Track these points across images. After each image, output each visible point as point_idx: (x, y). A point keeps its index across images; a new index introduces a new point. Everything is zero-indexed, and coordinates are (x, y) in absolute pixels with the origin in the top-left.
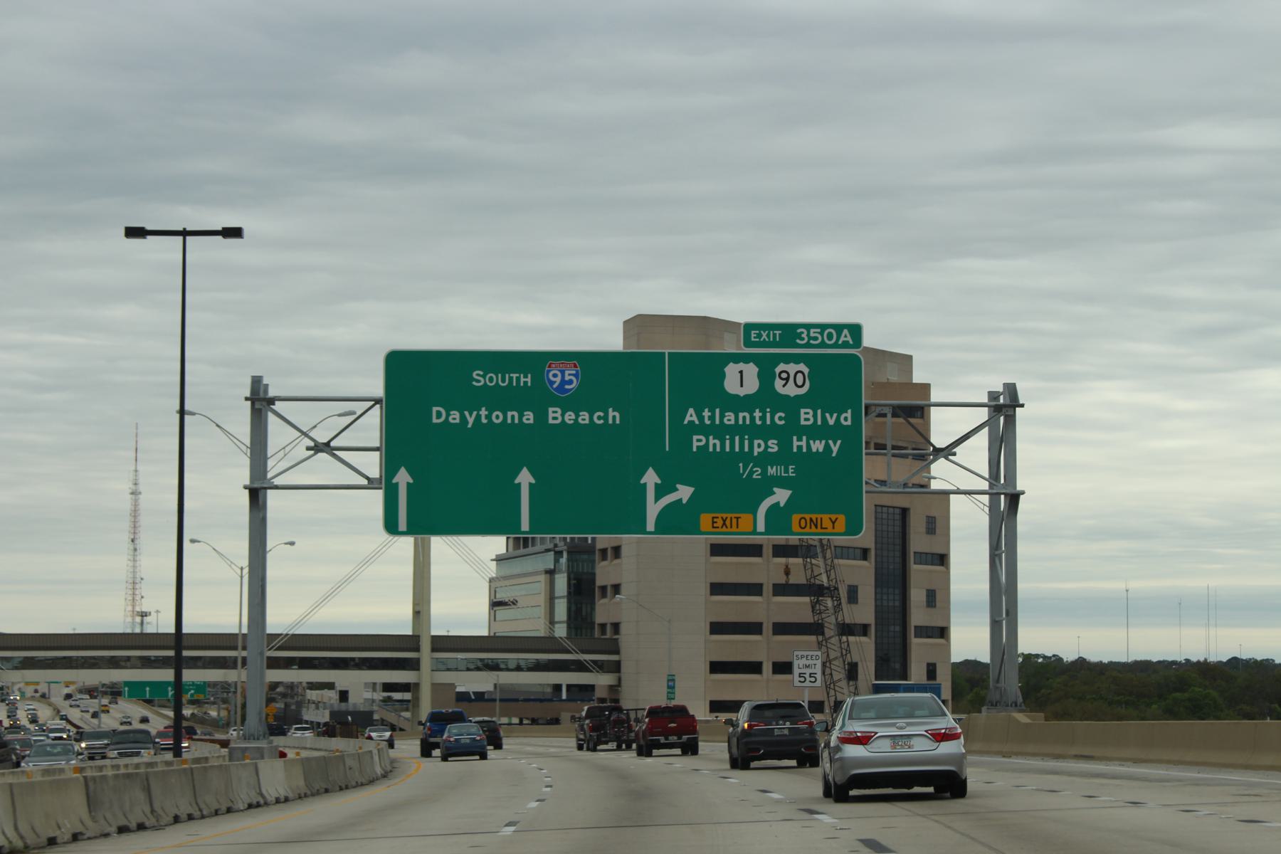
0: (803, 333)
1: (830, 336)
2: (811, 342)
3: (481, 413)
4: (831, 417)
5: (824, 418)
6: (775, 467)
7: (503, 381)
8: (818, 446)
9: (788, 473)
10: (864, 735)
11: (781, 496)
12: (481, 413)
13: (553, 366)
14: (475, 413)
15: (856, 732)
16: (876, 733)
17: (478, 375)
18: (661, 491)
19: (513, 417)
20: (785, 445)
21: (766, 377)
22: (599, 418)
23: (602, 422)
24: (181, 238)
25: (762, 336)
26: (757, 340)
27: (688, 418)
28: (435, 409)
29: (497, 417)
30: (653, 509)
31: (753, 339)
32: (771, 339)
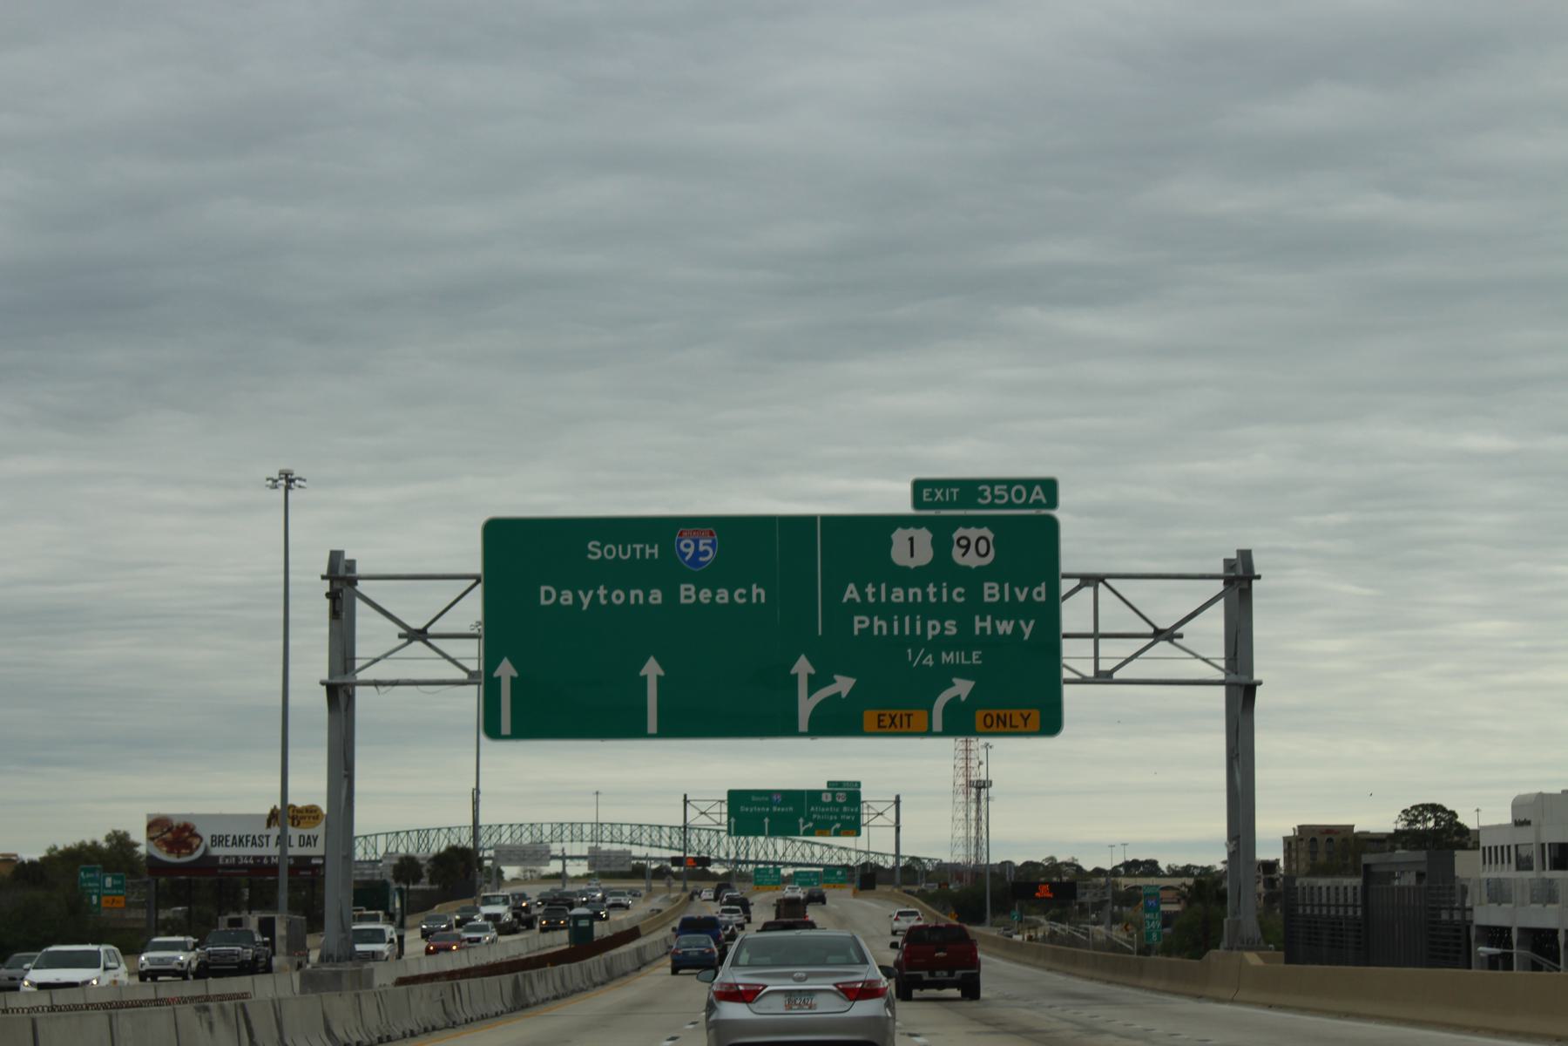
2: (997, 501)
4: (1021, 592)
5: (1012, 594)
6: (952, 654)
7: (625, 553)
9: (971, 659)
10: (748, 988)
11: (962, 688)
13: (685, 534)
14: (591, 593)
15: (737, 985)
16: (765, 986)
17: (594, 546)
18: (815, 684)
19: (637, 597)
20: (965, 625)
21: (942, 545)
22: (741, 596)
23: (744, 600)
24: (1101, 630)
25: (936, 495)
26: (931, 500)
27: (847, 596)
28: (543, 589)
29: (618, 597)
30: (806, 706)
32: (947, 499)
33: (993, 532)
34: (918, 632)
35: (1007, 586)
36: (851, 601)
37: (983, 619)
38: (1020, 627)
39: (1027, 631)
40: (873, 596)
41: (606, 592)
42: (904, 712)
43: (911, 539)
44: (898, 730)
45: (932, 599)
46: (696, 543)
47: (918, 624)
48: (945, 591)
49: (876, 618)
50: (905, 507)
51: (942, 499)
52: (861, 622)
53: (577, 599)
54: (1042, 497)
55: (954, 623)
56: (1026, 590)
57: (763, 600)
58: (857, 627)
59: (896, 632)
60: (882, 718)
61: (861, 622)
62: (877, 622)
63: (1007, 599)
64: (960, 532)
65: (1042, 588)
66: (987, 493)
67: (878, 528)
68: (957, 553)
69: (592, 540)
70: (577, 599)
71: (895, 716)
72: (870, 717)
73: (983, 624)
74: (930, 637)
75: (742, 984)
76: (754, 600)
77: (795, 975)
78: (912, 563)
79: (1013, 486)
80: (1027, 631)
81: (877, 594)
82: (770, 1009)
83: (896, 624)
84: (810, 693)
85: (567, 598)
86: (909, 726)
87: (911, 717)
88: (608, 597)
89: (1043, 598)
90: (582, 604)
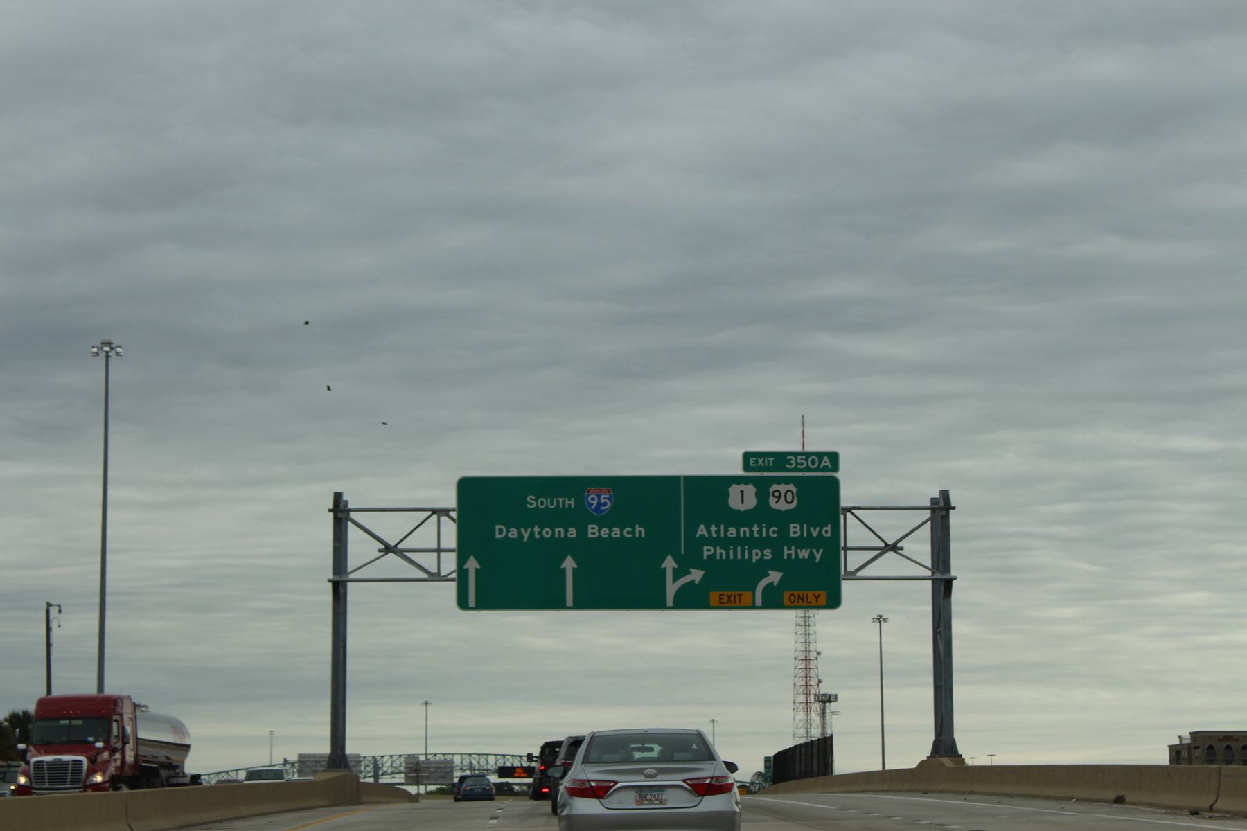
0: (791, 459)
1: (813, 462)
2: (799, 467)
3: (534, 530)
4: (815, 530)
5: (809, 531)
7: (552, 504)
8: (804, 554)
10: (600, 784)
11: (775, 577)
12: (534, 530)
14: (529, 530)
15: (589, 781)
16: (616, 783)
17: (531, 499)
18: (677, 574)
19: (559, 532)
20: (777, 552)
21: (762, 495)
22: (628, 532)
23: (630, 536)
25: (758, 462)
27: (699, 533)
28: (497, 527)
29: (547, 533)
30: (671, 589)
31: (752, 465)
32: (766, 465)
33: (796, 487)
34: (747, 557)
35: (805, 526)
36: (702, 536)
37: (789, 549)
38: (813, 553)
39: (818, 557)
40: (758, 533)
41: (539, 530)
42: (736, 593)
43: (742, 492)
44: (733, 605)
45: (756, 535)
46: (599, 497)
47: (746, 551)
48: (764, 529)
49: (718, 548)
50: (739, 471)
51: (763, 465)
52: (708, 550)
53: (520, 534)
54: (828, 464)
55: (770, 551)
56: (818, 529)
57: (643, 535)
58: (705, 554)
59: (732, 557)
60: (722, 597)
61: (708, 550)
62: (719, 551)
63: (805, 535)
64: (775, 487)
65: (829, 528)
66: (792, 462)
67: (716, 486)
68: (772, 501)
69: (534, 508)
70: (520, 534)
71: (731, 596)
72: (714, 596)
73: (789, 552)
74: (754, 561)
75: (593, 781)
76: (637, 535)
77: (646, 772)
78: (742, 508)
79: (810, 456)
80: (818, 557)
81: (718, 532)
82: (621, 805)
83: (731, 552)
84: (675, 579)
85: (513, 533)
86: (740, 602)
87: (742, 597)
88: (540, 533)
89: (829, 535)
90: (523, 537)
